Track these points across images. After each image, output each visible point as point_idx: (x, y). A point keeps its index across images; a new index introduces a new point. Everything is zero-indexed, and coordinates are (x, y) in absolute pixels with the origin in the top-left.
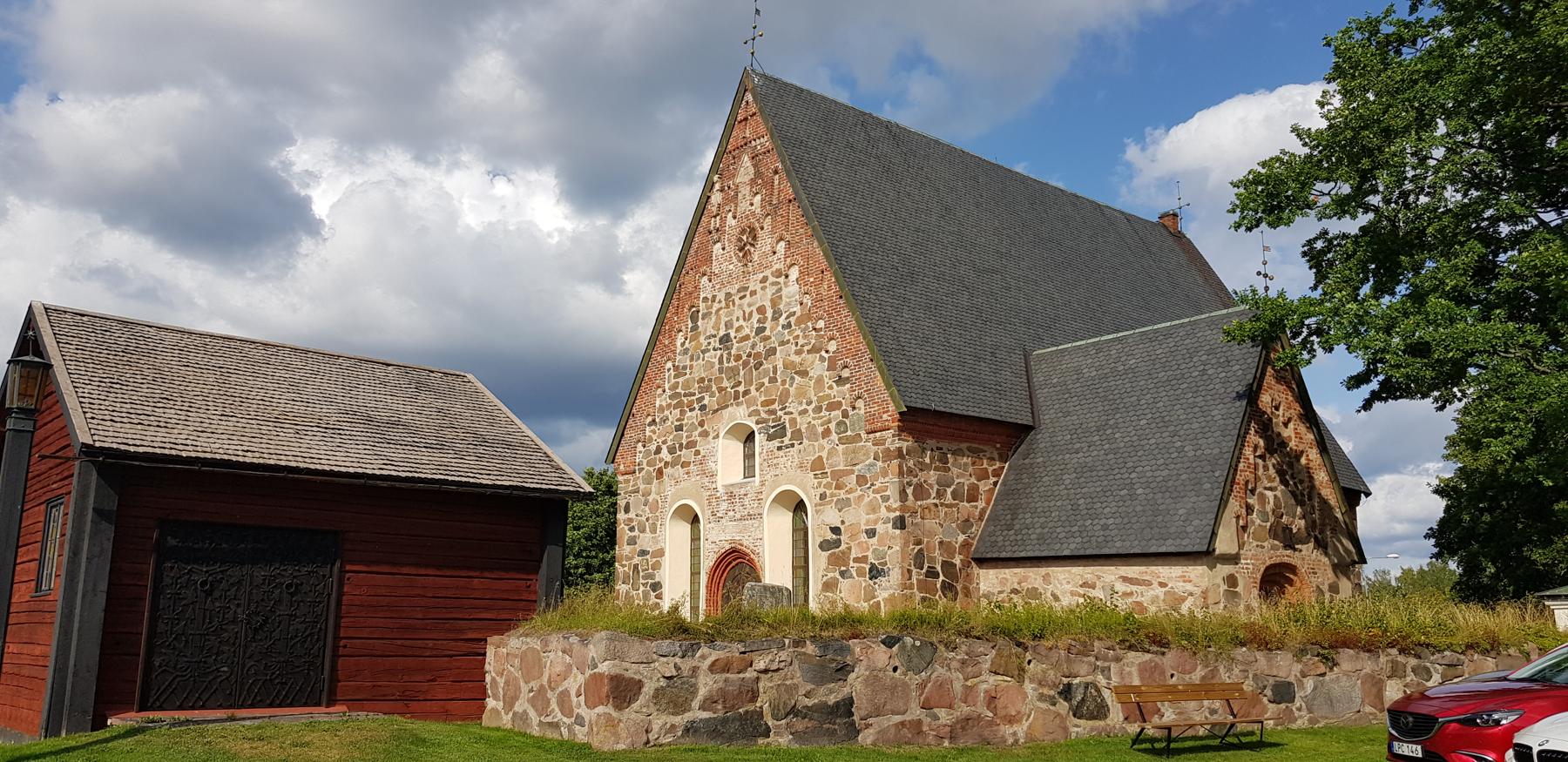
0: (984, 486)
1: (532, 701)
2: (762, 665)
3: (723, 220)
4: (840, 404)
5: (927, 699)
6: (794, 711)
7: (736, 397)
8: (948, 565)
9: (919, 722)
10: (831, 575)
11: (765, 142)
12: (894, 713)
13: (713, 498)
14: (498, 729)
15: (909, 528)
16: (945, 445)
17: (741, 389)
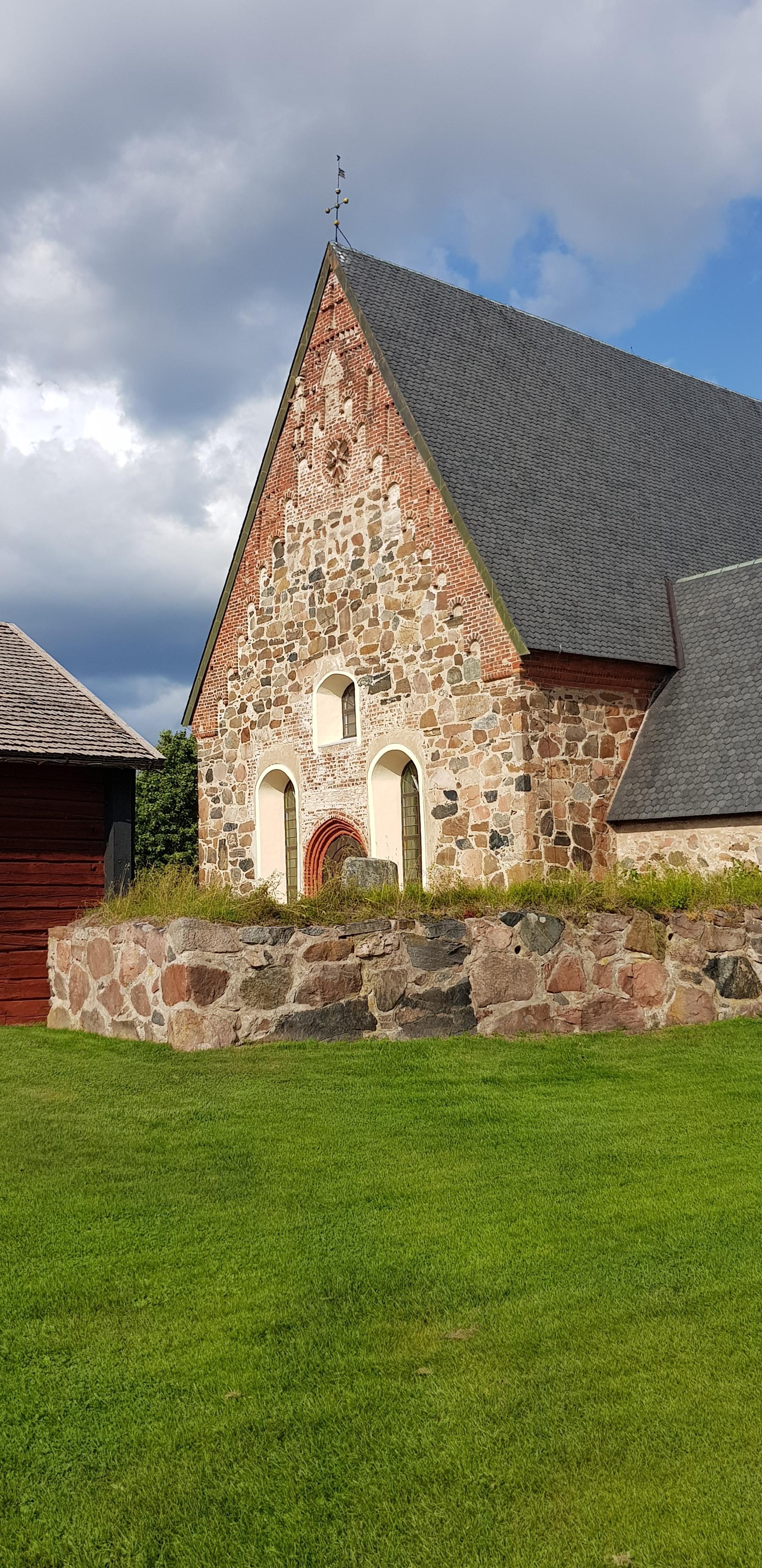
0: (620, 739)
1: (103, 999)
2: (365, 950)
3: (309, 432)
5: (554, 981)
6: (403, 1000)
7: (332, 644)
8: (580, 830)
9: (546, 1007)
10: (446, 845)
11: (355, 335)
12: (517, 998)
13: (309, 763)
14: (65, 1031)
15: (536, 790)
16: (575, 692)
17: (337, 634)
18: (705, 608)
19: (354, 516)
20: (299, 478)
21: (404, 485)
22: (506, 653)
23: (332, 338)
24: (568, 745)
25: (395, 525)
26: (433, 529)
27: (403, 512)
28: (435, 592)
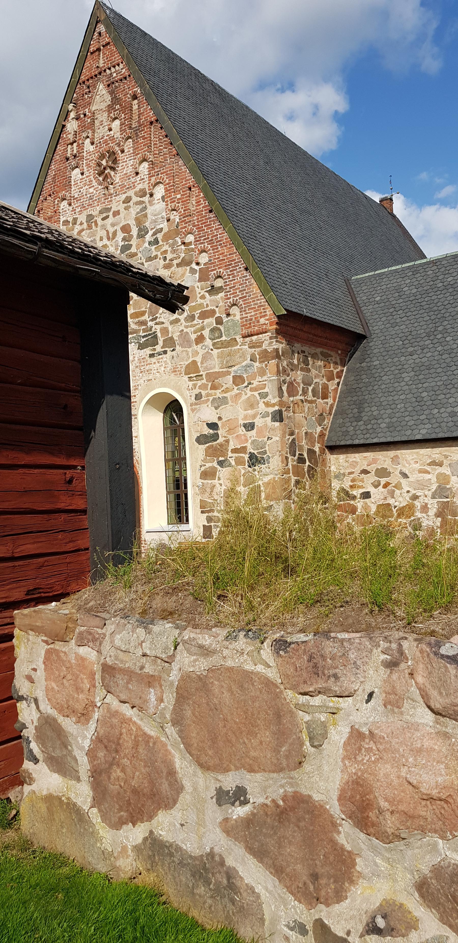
0: (332, 385)
3: (81, 147)
4: (213, 312)
8: (311, 452)
10: (208, 465)
11: (122, 70)
15: (286, 421)
16: (306, 348)
18: (380, 295)
19: (122, 210)
20: (73, 183)
21: (168, 184)
22: (263, 314)
23: (100, 73)
24: (303, 388)
25: (160, 216)
26: (195, 218)
27: (167, 205)
28: (197, 268)
